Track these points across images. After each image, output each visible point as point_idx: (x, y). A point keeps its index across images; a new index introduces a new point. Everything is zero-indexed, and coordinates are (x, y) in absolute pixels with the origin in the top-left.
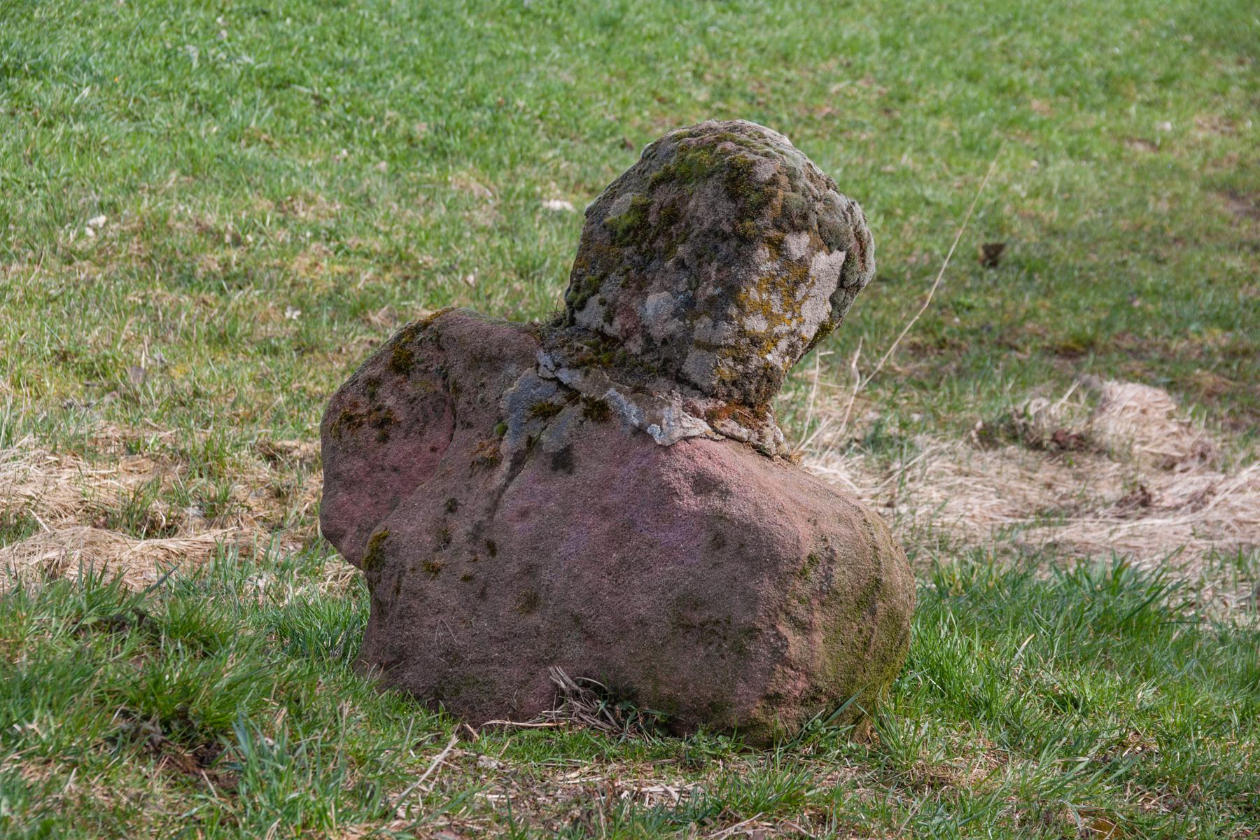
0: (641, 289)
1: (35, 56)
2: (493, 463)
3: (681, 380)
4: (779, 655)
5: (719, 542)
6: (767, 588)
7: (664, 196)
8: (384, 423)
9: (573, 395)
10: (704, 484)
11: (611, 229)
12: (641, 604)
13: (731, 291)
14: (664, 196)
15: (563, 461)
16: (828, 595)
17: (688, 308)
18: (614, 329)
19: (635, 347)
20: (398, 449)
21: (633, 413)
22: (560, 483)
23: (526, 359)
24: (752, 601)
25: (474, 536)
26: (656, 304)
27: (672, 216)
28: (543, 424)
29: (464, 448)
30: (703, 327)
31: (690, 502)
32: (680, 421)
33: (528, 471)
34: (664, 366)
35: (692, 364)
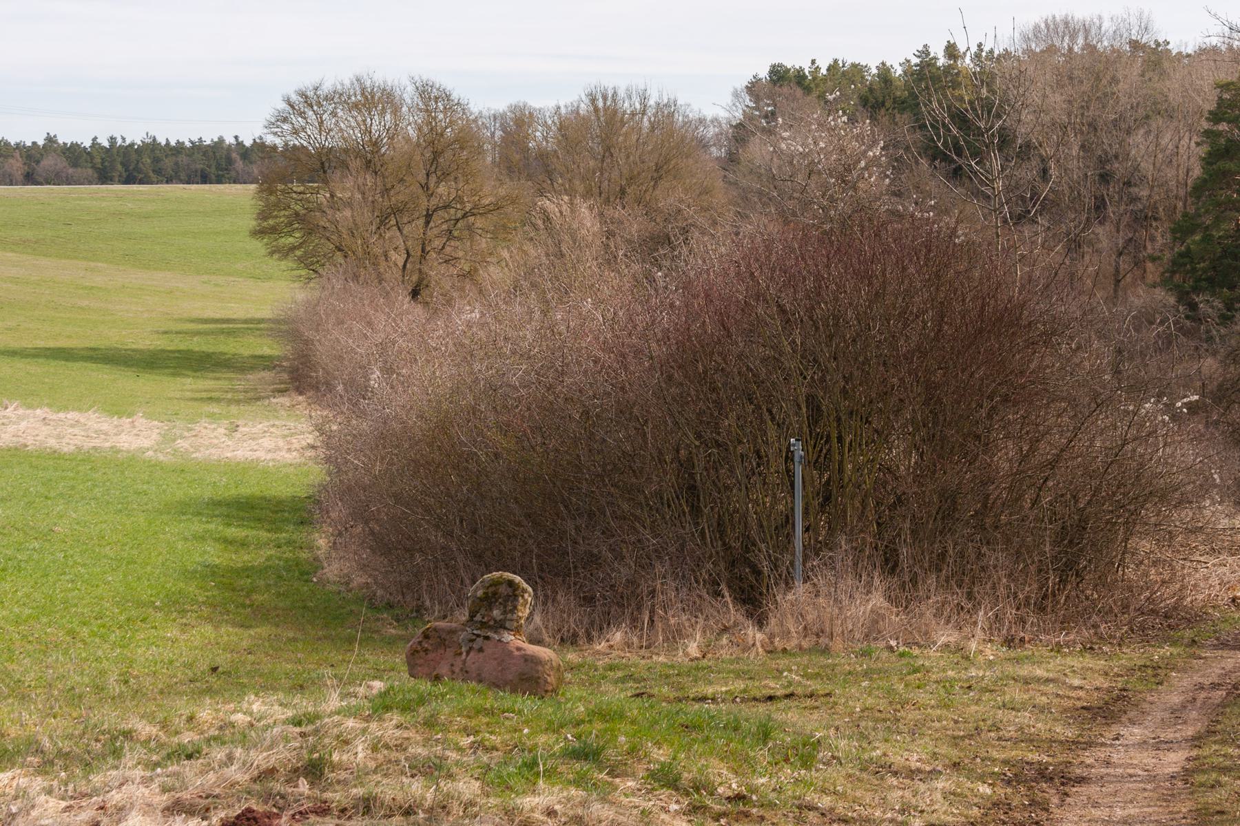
0: (491, 610)
1: (1075, 245)
2: (461, 654)
3: (505, 628)
4: (546, 681)
5: (526, 660)
6: (540, 668)
7: (491, 590)
8: (426, 651)
9: (478, 636)
10: (519, 649)
11: (480, 599)
12: (510, 677)
13: (515, 607)
14: (491, 590)
15: (481, 650)
16: (552, 668)
17: (505, 613)
18: (485, 620)
19: (492, 623)
20: (431, 656)
21: (496, 637)
22: (481, 655)
23: (463, 630)
24: (537, 671)
25: (462, 670)
26: (496, 613)
27: (495, 594)
28: (403, 680)
29: (450, 653)
30: (509, 616)
31: (517, 653)
32: (508, 637)
33: (472, 654)
34: (500, 626)
35: (507, 625)
